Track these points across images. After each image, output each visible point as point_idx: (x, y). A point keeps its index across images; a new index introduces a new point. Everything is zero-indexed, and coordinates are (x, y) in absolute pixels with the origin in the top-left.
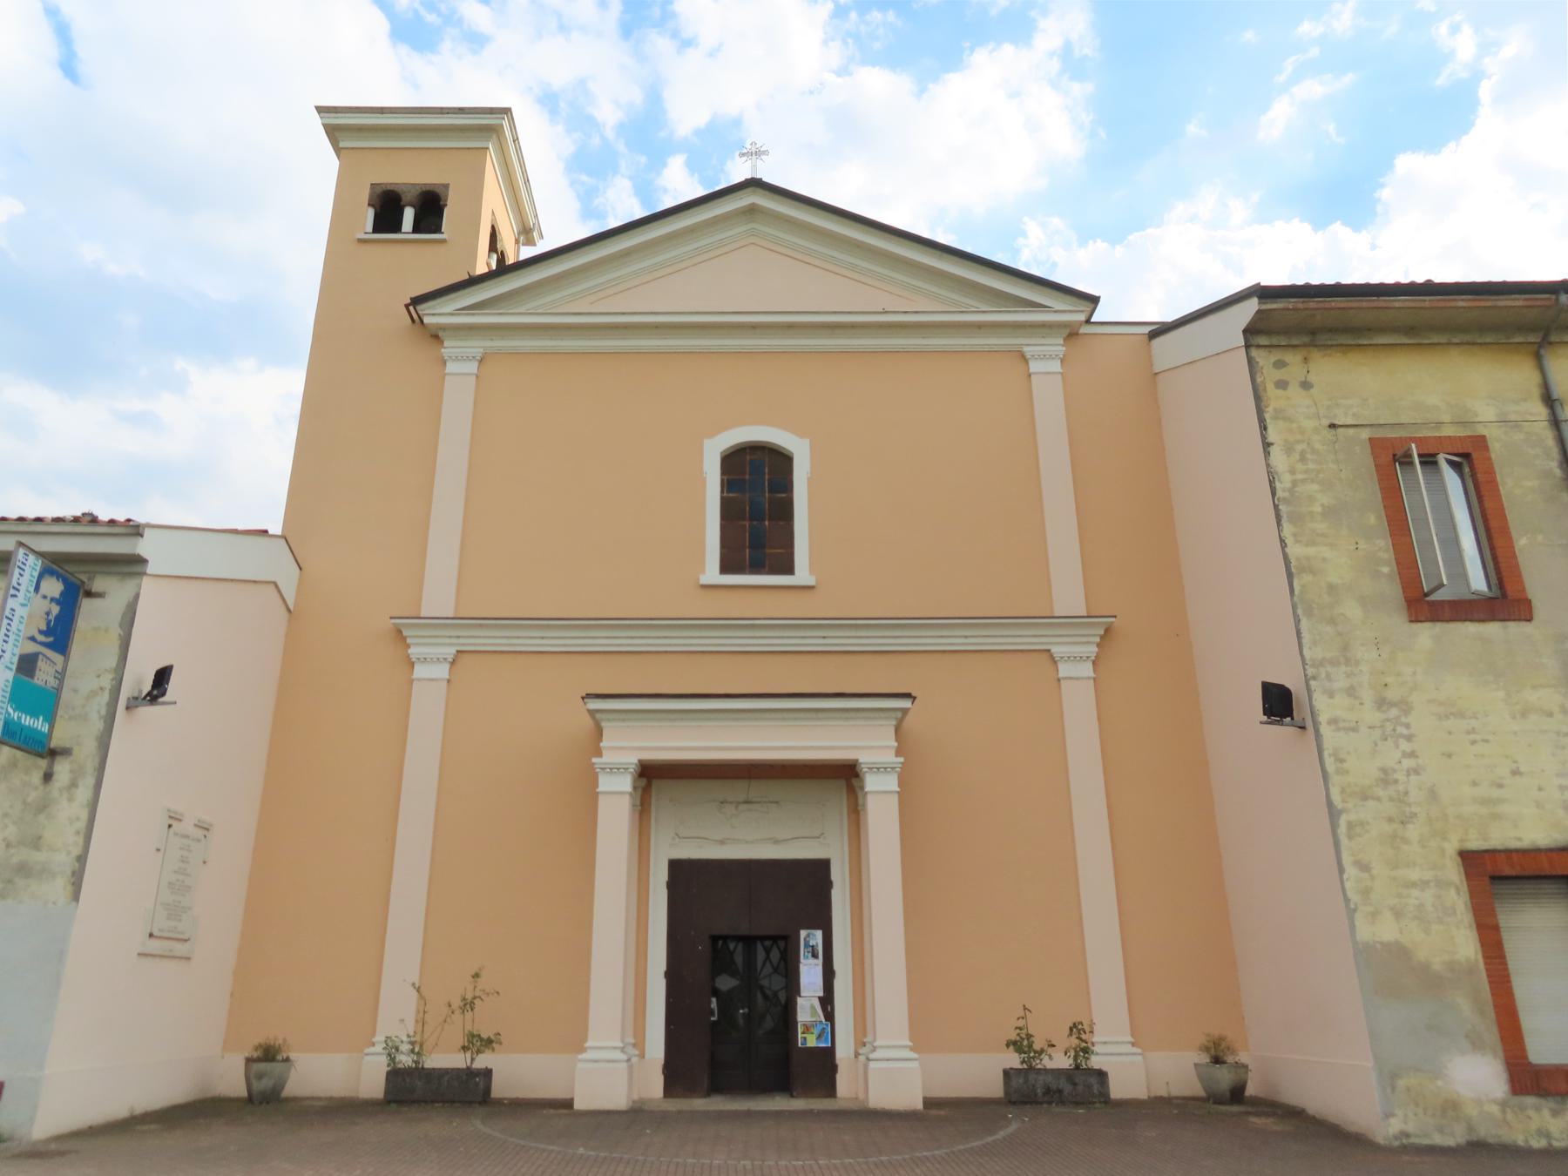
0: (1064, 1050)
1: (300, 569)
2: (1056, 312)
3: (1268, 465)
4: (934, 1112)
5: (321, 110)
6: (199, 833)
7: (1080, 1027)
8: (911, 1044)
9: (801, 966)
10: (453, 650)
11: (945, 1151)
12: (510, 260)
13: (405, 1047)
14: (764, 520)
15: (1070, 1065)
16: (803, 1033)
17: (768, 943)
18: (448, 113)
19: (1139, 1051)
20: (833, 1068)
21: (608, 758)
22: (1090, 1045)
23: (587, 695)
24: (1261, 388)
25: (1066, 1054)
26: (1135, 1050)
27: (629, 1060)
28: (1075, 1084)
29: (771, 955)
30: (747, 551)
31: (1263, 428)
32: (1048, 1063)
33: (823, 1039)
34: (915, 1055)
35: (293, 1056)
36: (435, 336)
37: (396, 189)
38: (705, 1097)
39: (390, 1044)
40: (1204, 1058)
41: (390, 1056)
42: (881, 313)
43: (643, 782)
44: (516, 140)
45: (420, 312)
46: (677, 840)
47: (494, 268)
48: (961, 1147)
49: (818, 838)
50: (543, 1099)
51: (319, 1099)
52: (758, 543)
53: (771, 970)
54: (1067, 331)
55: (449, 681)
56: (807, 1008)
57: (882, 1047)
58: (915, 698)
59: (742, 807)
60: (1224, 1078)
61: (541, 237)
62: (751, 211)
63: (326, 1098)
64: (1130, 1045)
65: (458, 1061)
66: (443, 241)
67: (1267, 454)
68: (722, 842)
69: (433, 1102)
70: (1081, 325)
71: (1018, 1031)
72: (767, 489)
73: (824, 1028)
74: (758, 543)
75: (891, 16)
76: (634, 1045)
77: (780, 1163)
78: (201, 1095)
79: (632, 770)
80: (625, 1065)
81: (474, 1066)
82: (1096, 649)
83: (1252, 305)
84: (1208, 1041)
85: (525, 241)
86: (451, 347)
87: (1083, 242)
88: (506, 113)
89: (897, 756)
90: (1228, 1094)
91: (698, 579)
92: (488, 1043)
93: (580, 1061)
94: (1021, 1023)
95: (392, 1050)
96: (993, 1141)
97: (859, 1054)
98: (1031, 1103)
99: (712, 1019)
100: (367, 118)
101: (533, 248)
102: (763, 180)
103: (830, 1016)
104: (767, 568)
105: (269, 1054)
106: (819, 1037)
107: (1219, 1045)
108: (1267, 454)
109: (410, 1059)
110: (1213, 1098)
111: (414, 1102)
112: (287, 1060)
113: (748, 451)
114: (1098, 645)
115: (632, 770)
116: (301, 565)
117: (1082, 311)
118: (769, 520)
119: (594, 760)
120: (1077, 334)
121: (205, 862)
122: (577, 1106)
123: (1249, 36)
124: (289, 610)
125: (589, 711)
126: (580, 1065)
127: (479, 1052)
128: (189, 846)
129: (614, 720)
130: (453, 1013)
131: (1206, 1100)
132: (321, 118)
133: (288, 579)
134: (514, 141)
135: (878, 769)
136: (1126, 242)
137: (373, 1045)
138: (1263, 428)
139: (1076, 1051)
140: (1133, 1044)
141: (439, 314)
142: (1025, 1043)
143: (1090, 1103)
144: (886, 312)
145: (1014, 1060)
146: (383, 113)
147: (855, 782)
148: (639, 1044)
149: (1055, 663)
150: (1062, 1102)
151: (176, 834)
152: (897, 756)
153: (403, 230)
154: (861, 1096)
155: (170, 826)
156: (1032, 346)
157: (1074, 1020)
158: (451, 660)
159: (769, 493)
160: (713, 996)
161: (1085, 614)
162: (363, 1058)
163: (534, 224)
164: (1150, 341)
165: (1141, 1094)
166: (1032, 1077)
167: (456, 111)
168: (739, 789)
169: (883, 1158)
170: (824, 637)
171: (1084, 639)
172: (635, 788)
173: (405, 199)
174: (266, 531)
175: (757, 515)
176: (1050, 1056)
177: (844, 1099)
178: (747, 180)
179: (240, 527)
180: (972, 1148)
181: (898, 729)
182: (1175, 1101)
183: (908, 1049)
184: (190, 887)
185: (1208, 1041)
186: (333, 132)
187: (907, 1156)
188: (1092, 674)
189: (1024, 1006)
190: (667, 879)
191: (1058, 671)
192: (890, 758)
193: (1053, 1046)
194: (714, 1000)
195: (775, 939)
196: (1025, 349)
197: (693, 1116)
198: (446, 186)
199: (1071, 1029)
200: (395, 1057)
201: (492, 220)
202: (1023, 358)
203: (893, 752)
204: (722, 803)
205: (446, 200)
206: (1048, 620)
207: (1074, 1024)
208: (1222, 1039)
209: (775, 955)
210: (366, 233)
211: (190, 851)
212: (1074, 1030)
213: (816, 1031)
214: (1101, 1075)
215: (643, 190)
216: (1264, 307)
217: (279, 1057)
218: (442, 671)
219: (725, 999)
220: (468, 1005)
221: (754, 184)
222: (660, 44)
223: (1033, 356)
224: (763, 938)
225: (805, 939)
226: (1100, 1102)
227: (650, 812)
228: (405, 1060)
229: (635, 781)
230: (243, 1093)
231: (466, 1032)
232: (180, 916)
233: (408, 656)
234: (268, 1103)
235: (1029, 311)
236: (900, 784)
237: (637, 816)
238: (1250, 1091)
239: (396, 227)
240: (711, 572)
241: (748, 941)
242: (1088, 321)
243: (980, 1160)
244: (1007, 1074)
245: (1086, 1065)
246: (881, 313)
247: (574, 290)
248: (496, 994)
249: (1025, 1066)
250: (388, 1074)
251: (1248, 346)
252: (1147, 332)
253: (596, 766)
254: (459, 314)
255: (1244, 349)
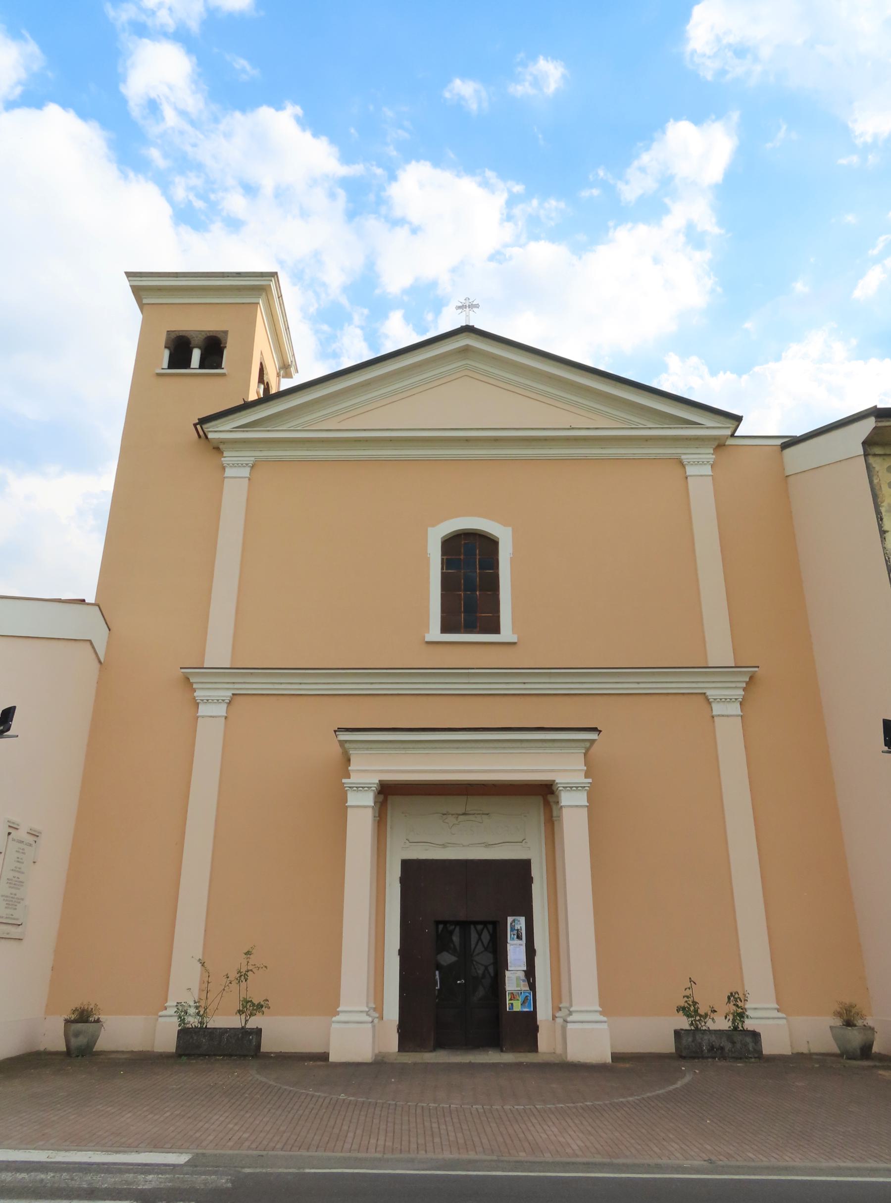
0: (725, 1014)
1: (110, 630)
2: (707, 428)
3: (884, 548)
4: (621, 1065)
5: (129, 275)
6: (31, 839)
7: (737, 996)
8: (601, 1009)
9: (508, 945)
10: (229, 693)
11: (636, 1097)
12: (273, 390)
13: (192, 1011)
14: (477, 591)
15: (730, 1027)
16: (511, 1000)
17: (480, 927)
18: (228, 277)
19: (784, 1015)
20: (536, 1029)
21: (355, 779)
22: (744, 1011)
23: (338, 728)
24: (877, 488)
25: (726, 1017)
26: (780, 1015)
27: (372, 1022)
28: (733, 1043)
29: (482, 937)
30: (463, 615)
31: (880, 519)
32: (711, 1025)
33: (527, 1004)
34: (605, 1019)
35: (103, 1018)
36: (217, 448)
37: (186, 335)
38: (431, 1051)
39: (181, 1008)
40: (838, 1022)
41: (181, 1018)
42: (568, 429)
43: (381, 797)
44: (280, 297)
45: (205, 430)
46: (408, 844)
47: (262, 396)
48: (649, 1094)
49: (521, 842)
50: (309, 1053)
51: (123, 1052)
52: (471, 608)
53: (483, 949)
54: (716, 444)
55: (226, 718)
56: (514, 979)
57: (577, 1011)
58: (600, 731)
59: (461, 818)
60: (855, 1038)
61: (297, 371)
62: (465, 351)
63: (128, 1052)
64: (776, 1011)
65: (234, 1022)
66: (224, 375)
67: (883, 539)
68: (444, 846)
69: (215, 1055)
70: (727, 438)
71: (686, 999)
72: (478, 566)
73: (527, 996)
74: (471, 608)
75: (562, 205)
76: (375, 1009)
77: (504, 1107)
78: (28, 1050)
79: (374, 789)
80: (370, 1025)
81: (247, 1026)
82: (743, 693)
83: (870, 424)
84: (841, 1008)
85: (284, 375)
86: (229, 457)
87: (714, 373)
88: (273, 277)
89: (586, 777)
90: (859, 1051)
91: (424, 637)
92: (259, 1008)
93: (333, 1022)
94: (688, 992)
95: (182, 1014)
96: (674, 1089)
97: (556, 1017)
98: (698, 1058)
99: (437, 988)
100: (258, 280)
101: (291, 379)
102: (475, 326)
103: (532, 987)
104: (478, 629)
105: (83, 1016)
106: (523, 1003)
107: (850, 1011)
108: (883, 539)
109: (196, 1020)
110: (846, 1054)
111: (200, 1055)
112: (98, 1021)
113: (463, 536)
114: (744, 689)
115: (374, 789)
116: (110, 628)
117: (729, 428)
118: (480, 591)
119: (344, 781)
120: (724, 445)
121: (34, 862)
122: (332, 1059)
123: (850, 218)
124: (100, 662)
125: (340, 741)
126: (334, 1026)
127: (251, 1015)
128: (23, 849)
129: (360, 749)
130: (231, 983)
131: (840, 1056)
132: (129, 281)
133: (100, 637)
134: (279, 298)
135: (571, 788)
136: (751, 372)
137: (166, 1009)
138: (880, 519)
139: (734, 1016)
140: (778, 1010)
141: (219, 431)
142: (692, 1008)
143: (747, 1058)
144: (573, 428)
145: (684, 1023)
146: (177, 277)
147: (550, 798)
148: (379, 1008)
149: (710, 703)
150: (724, 1058)
151: (13, 840)
152: (586, 777)
153: (192, 367)
154: (559, 1050)
155: (9, 834)
156: (688, 455)
157: (731, 991)
158: (228, 701)
159: (479, 570)
160: (437, 970)
161: (734, 666)
162: (157, 1020)
163: (291, 362)
164: (782, 451)
165: (787, 1051)
166: (698, 1037)
167: (235, 275)
168: (457, 804)
169: (588, 1103)
170: (524, 683)
171: (733, 685)
172: (375, 803)
173: (193, 343)
174: (84, 600)
175: (470, 586)
176: (713, 1019)
177: (545, 1053)
178: (462, 327)
179: (63, 598)
180: (658, 1096)
181: (585, 754)
182: (815, 1057)
183: (598, 1014)
184: (22, 882)
185: (841, 1008)
186: (137, 291)
187: (607, 1102)
188: (740, 713)
189: (690, 978)
190: (400, 876)
191: (712, 710)
192: (580, 779)
193: (715, 1011)
194: (437, 973)
195: (485, 923)
196: (683, 457)
197: (427, 1068)
198: (226, 332)
199: (729, 998)
200: (184, 1019)
201: (261, 358)
202: (682, 465)
203: (583, 774)
204: (444, 814)
205: (226, 343)
206: (705, 669)
207: (731, 994)
208: (852, 1006)
209: (486, 937)
210: (163, 369)
211: (23, 853)
212: (732, 998)
213: (521, 999)
214: (755, 1036)
215: (371, 337)
216: (880, 424)
217: (92, 1019)
218: (221, 710)
219: (448, 973)
220: (243, 976)
221: (468, 330)
222: (371, 223)
223: (689, 462)
224: (475, 923)
225: (511, 924)
226: (755, 1058)
227: (386, 819)
228: (193, 1021)
229: (376, 797)
230: (63, 1048)
231: (242, 999)
232: (16, 906)
233: (194, 698)
234: (83, 1056)
235: (687, 427)
236: (589, 799)
237: (376, 824)
238: (875, 1049)
239: (186, 364)
240: (434, 633)
241: (465, 925)
242: (732, 436)
243: (668, 1106)
244: (678, 1034)
245: (742, 1027)
246: (568, 429)
247: (325, 412)
248: (264, 968)
249: (693, 1028)
250: (179, 1032)
251: (866, 455)
252: (780, 444)
253: (559, 786)
254: (236, 431)
255: (863, 457)
